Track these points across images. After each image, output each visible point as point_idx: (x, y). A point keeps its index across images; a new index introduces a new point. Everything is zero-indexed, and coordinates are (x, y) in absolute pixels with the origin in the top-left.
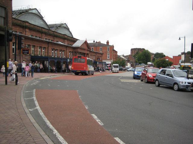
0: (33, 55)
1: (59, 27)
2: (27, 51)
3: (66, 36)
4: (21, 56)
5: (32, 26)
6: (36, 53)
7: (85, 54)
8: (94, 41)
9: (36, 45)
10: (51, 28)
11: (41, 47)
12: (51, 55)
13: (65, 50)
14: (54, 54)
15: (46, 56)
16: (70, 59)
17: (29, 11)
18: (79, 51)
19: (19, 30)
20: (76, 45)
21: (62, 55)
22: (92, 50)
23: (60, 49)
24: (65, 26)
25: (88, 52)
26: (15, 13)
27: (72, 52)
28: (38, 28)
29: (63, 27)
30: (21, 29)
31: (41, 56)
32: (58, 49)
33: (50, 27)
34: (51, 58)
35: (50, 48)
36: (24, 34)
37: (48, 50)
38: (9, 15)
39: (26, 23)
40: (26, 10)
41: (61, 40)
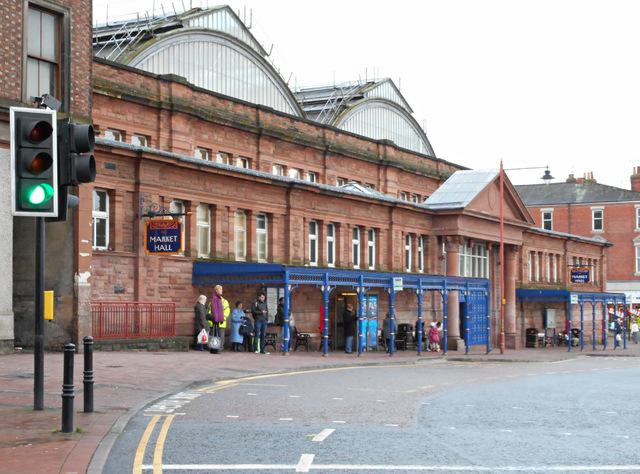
0: (204, 256)
1: (355, 99)
2: (170, 233)
3: (391, 152)
4: (141, 263)
5: (205, 102)
6: (219, 247)
7: (496, 246)
8: (547, 176)
9: (220, 203)
10: (306, 109)
11: (248, 213)
12: (301, 255)
13: (383, 227)
14: (309, 247)
15: (276, 261)
16: (413, 279)
17: (188, 21)
18: (464, 229)
19: (134, 124)
20: (440, 197)
21: (363, 255)
22: (548, 226)
23: (353, 223)
24: (385, 92)
25: (515, 238)
26: (118, 36)
27: (424, 237)
28: (240, 110)
29: (379, 100)
30: (150, 119)
31: (250, 262)
32: (342, 221)
33: (305, 104)
34: (300, 268)
35: (296, 217)
36: (163, 143)
37: (287, 231)
38: (80, 48)
39: (173, 85)
40: (175, 17)
41: (363, 171)
